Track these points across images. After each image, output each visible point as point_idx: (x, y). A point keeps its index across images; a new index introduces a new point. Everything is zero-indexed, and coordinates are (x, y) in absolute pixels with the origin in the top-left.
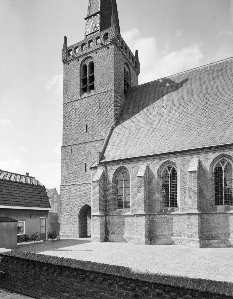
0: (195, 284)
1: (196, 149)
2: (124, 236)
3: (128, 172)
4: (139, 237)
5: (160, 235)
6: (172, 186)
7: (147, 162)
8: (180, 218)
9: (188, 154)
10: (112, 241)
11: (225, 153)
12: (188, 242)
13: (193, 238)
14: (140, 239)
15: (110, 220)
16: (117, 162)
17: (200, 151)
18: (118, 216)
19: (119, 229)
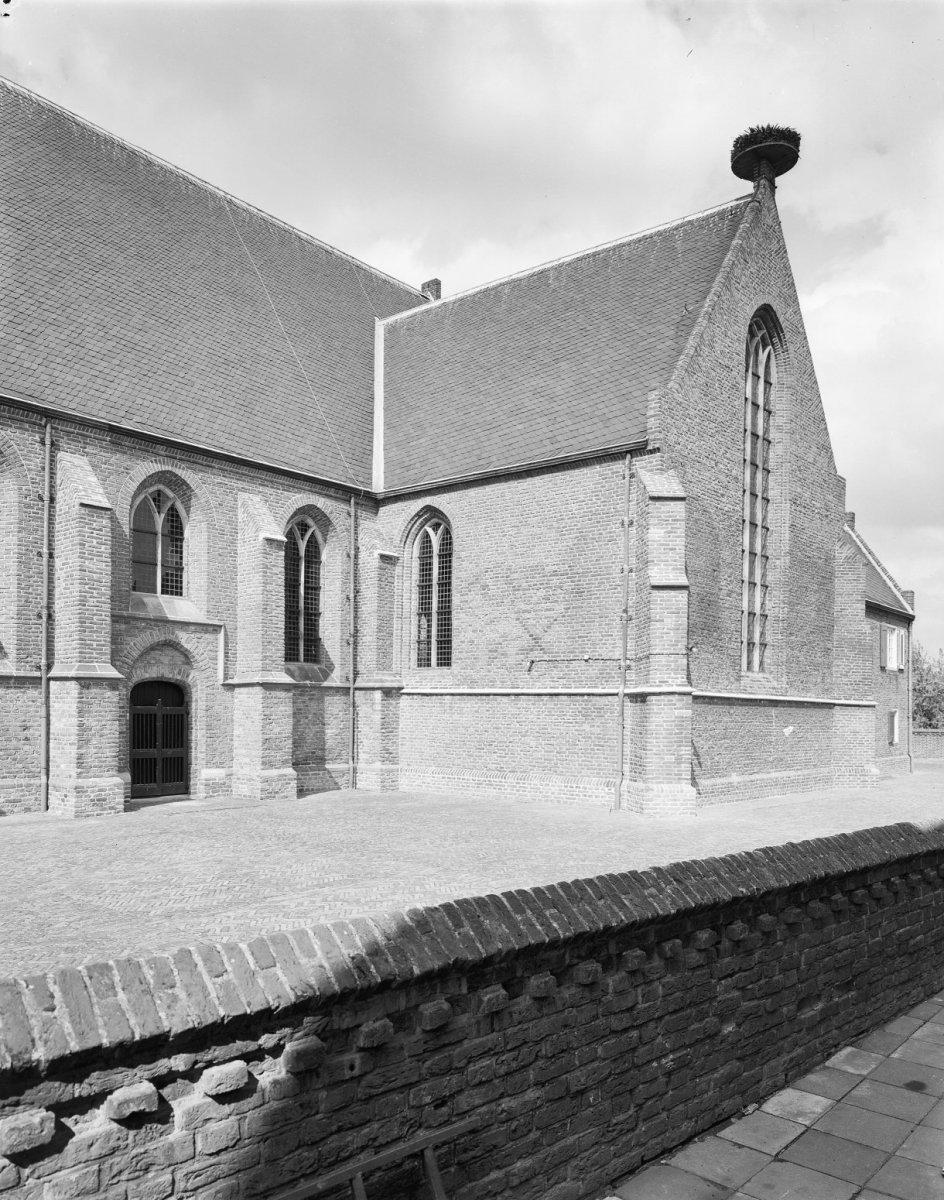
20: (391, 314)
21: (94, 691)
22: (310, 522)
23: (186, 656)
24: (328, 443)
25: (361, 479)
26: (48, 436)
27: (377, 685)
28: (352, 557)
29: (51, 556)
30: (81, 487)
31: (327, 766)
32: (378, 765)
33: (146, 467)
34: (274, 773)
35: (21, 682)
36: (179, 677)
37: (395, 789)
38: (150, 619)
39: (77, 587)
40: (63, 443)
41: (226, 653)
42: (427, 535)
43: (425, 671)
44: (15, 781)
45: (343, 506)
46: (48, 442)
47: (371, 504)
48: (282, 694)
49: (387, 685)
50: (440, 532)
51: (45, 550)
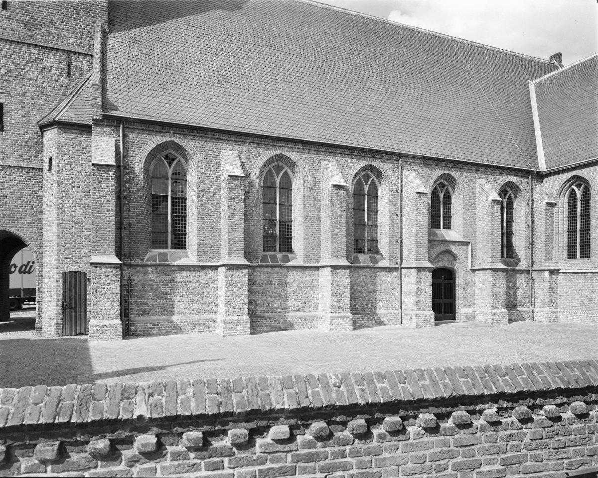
0: (367, 393)
1: (286, 138)
2: (177, 318)
3: (183, 161)
4: (236, 318)
5: (264, 312)
6: (176, 202)
7: (237, 147)
8: (302, 276)
9: (319, 151)
10: (141, 333)
11: (374, 164)
12: (334, 321)
13: (342, 312)
14: (238, 323)
15: (135, 277)
16: (158, 128)
17: (339, 151)
18: (159, 268)
19: (163, 301)
20: (537, 78)
21: (422, 273)
22: (508, 189)
23: (454, 257)
24: (515, 149)
25: (533, 165)
26: (400, 164)
27: (546, 269)
28: (530, 204)
29: (401, 215)
30: (415, 185)
31: (518, 309)
32: (547, 309)
33: (438, 173)
34: (498, 311)
35: (391, 269)
36: (451, 266)
37: (556, 321)
38: (440, 241)
39: (414, 228)
40: (405, 167)
41: (472, 255)
42: (573, 190)
43: (573, 261)
44: (389, 311)
45: (525, 180)
46: (400, 167)
47: (539, 177)
48: (501, 274)
49: (552, 268)
50: (581, 188)
51: (399, 213)
